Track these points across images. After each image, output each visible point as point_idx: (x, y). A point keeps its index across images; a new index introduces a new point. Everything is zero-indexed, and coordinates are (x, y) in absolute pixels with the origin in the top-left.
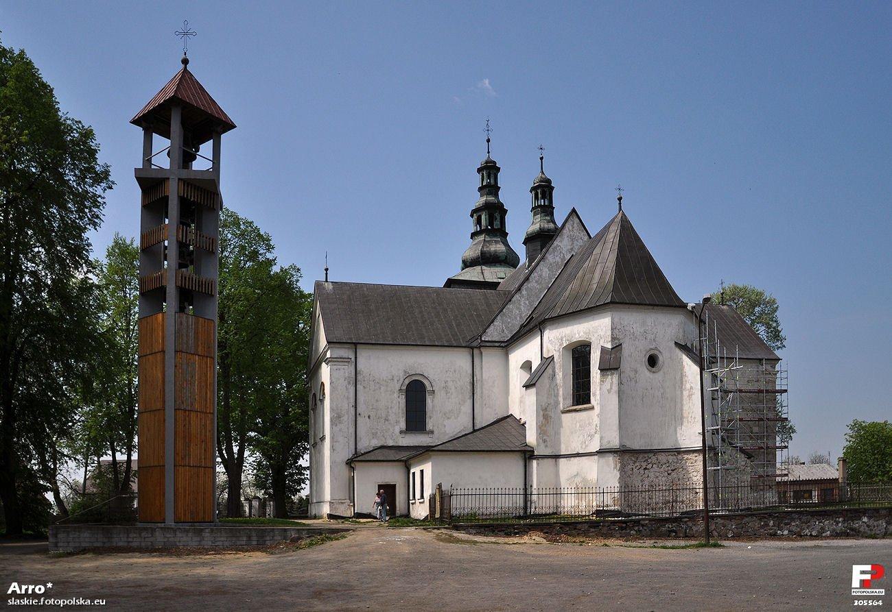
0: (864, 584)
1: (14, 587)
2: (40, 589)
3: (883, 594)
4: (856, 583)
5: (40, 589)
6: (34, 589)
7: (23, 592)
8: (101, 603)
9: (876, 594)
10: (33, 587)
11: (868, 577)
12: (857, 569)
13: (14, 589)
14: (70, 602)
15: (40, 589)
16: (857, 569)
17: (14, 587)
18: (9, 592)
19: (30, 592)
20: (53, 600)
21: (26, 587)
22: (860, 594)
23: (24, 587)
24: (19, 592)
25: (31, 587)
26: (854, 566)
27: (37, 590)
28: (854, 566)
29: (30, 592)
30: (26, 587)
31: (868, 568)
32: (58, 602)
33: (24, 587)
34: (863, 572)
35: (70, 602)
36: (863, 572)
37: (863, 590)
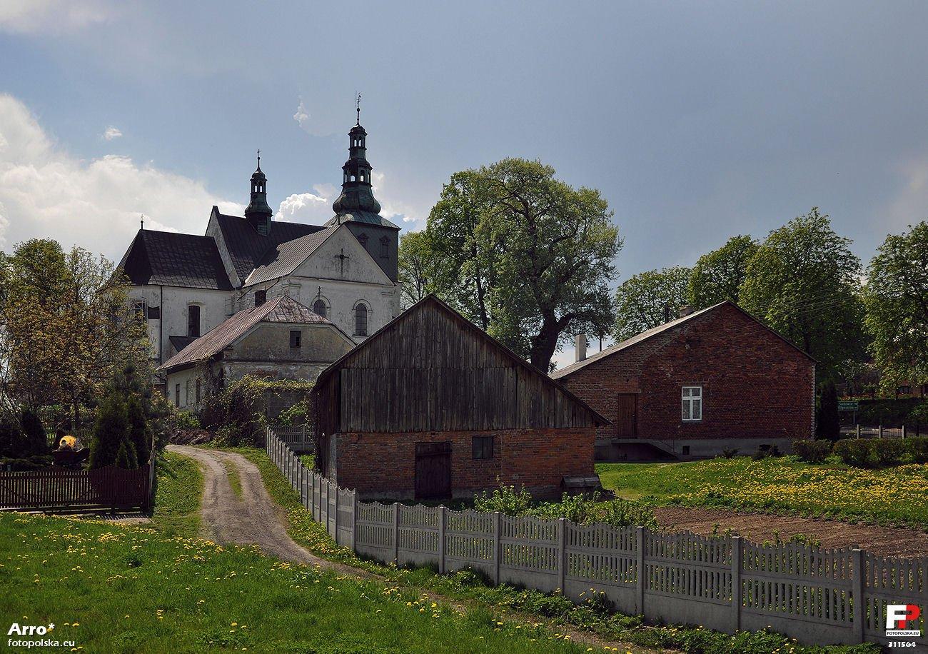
0: (898, 625)
1: (15, 628)
2: (42, 630)
3: (919, 635)
4: (890, 624)
5: (41, 630)
6: (35, 631)
7: (24, 633)
8: (70, 645)
9: (911, 635)
10: (35, 628)
11: (903, 617)
12: (891, 609)
13: (15, 630)
14: (38, 644)
15: (41, 630)
16: (891, 609)
17: (15, 628)
18: (10, 633)
19: (31, 633)
20: (20, 641)
21: (27, 628)
22: (895, 635)
23: (25, 628)
24: (19, 633)
25: (32, 628)
26: (888, 606)
27: (38, 631)
28: (888, 606)
29: (31, 633)
30: (27, 628)
31: (903, 608)
32: (25, 644)
33: (25, 628)
34: (897, 613)
35: (38, 644)
36: (897, 613)
37: (898, 631)
